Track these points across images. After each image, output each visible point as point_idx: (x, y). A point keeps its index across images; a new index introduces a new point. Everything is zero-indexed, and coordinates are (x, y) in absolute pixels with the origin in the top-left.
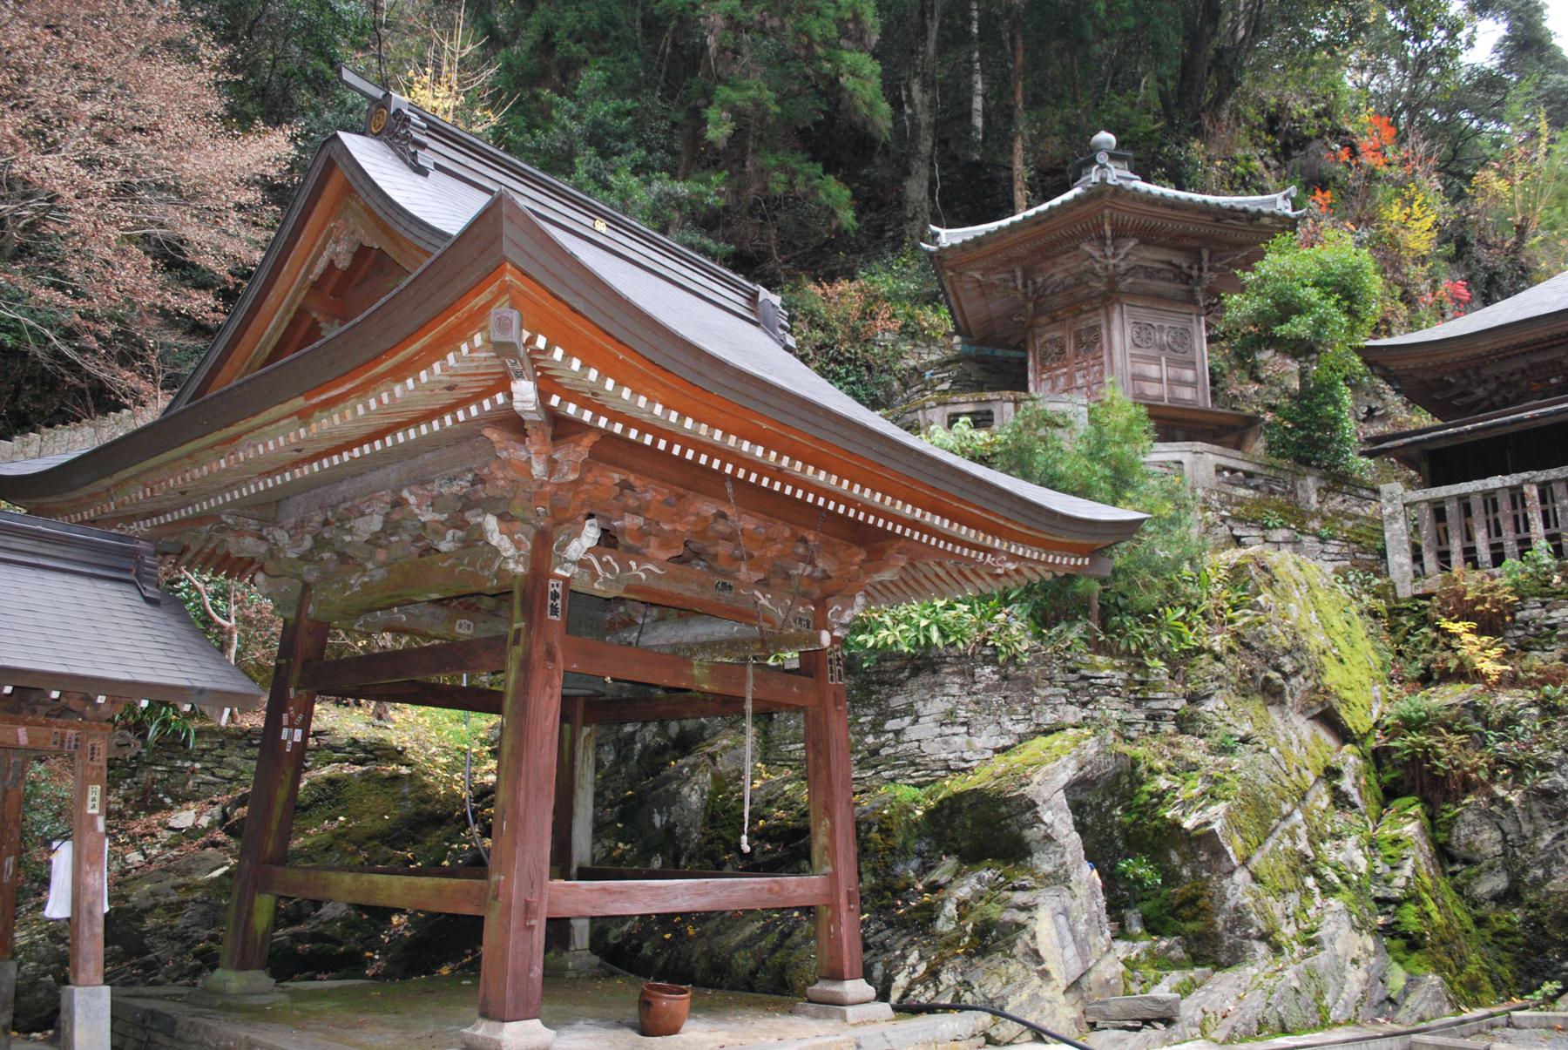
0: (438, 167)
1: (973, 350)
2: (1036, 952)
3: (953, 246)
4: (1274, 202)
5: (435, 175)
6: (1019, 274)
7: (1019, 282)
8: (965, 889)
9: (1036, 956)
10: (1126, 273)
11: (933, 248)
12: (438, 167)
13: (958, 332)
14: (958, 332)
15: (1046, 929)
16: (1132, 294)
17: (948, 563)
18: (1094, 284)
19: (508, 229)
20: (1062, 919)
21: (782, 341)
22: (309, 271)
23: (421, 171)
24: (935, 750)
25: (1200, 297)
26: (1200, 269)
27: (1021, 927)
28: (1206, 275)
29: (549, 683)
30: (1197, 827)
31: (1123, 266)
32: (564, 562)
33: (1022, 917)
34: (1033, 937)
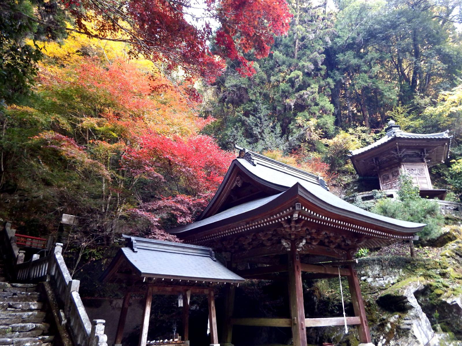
0: (258, 163)
1: (361, 178)
2: (415, 336)
3: (356, 155)
4: (443, 135)
5: (258, 165)
6: (374, 160)
7: (374, 161)
8: (392, 319)
9: (414, 337)
10: (404, 157)
11: (351, 156)
12: (258, 163)
13: (357, 174)
14: (357, 174)
15: (416, 330)
16: (406, 162)
17: (385, 241)
18: (395, 161)
19: (299, 189)
20: (419, 327)
21: (326, 188)
22: (231, 186)
23: (255, 165)
24: (375, 284)
25: (425, 160)
26: (424, 153)
27: (409, 329)
28: (426, 154)
29: (299, 273)
30: (452, 302)
31: (403, 155)
32: (298, 248)
33: (409, 327)
34: (413, 332)
